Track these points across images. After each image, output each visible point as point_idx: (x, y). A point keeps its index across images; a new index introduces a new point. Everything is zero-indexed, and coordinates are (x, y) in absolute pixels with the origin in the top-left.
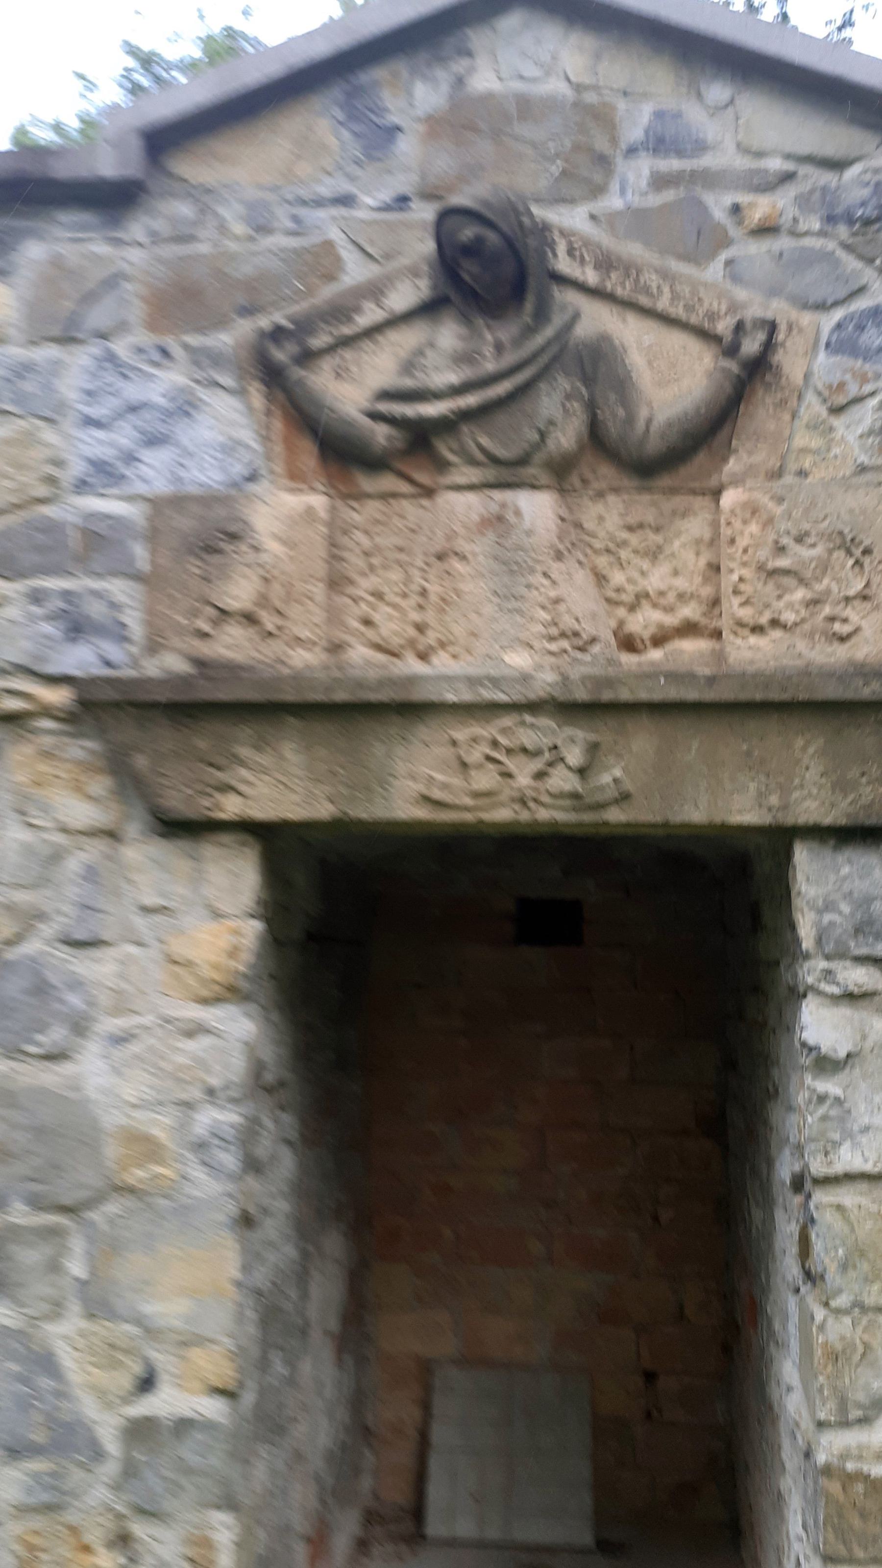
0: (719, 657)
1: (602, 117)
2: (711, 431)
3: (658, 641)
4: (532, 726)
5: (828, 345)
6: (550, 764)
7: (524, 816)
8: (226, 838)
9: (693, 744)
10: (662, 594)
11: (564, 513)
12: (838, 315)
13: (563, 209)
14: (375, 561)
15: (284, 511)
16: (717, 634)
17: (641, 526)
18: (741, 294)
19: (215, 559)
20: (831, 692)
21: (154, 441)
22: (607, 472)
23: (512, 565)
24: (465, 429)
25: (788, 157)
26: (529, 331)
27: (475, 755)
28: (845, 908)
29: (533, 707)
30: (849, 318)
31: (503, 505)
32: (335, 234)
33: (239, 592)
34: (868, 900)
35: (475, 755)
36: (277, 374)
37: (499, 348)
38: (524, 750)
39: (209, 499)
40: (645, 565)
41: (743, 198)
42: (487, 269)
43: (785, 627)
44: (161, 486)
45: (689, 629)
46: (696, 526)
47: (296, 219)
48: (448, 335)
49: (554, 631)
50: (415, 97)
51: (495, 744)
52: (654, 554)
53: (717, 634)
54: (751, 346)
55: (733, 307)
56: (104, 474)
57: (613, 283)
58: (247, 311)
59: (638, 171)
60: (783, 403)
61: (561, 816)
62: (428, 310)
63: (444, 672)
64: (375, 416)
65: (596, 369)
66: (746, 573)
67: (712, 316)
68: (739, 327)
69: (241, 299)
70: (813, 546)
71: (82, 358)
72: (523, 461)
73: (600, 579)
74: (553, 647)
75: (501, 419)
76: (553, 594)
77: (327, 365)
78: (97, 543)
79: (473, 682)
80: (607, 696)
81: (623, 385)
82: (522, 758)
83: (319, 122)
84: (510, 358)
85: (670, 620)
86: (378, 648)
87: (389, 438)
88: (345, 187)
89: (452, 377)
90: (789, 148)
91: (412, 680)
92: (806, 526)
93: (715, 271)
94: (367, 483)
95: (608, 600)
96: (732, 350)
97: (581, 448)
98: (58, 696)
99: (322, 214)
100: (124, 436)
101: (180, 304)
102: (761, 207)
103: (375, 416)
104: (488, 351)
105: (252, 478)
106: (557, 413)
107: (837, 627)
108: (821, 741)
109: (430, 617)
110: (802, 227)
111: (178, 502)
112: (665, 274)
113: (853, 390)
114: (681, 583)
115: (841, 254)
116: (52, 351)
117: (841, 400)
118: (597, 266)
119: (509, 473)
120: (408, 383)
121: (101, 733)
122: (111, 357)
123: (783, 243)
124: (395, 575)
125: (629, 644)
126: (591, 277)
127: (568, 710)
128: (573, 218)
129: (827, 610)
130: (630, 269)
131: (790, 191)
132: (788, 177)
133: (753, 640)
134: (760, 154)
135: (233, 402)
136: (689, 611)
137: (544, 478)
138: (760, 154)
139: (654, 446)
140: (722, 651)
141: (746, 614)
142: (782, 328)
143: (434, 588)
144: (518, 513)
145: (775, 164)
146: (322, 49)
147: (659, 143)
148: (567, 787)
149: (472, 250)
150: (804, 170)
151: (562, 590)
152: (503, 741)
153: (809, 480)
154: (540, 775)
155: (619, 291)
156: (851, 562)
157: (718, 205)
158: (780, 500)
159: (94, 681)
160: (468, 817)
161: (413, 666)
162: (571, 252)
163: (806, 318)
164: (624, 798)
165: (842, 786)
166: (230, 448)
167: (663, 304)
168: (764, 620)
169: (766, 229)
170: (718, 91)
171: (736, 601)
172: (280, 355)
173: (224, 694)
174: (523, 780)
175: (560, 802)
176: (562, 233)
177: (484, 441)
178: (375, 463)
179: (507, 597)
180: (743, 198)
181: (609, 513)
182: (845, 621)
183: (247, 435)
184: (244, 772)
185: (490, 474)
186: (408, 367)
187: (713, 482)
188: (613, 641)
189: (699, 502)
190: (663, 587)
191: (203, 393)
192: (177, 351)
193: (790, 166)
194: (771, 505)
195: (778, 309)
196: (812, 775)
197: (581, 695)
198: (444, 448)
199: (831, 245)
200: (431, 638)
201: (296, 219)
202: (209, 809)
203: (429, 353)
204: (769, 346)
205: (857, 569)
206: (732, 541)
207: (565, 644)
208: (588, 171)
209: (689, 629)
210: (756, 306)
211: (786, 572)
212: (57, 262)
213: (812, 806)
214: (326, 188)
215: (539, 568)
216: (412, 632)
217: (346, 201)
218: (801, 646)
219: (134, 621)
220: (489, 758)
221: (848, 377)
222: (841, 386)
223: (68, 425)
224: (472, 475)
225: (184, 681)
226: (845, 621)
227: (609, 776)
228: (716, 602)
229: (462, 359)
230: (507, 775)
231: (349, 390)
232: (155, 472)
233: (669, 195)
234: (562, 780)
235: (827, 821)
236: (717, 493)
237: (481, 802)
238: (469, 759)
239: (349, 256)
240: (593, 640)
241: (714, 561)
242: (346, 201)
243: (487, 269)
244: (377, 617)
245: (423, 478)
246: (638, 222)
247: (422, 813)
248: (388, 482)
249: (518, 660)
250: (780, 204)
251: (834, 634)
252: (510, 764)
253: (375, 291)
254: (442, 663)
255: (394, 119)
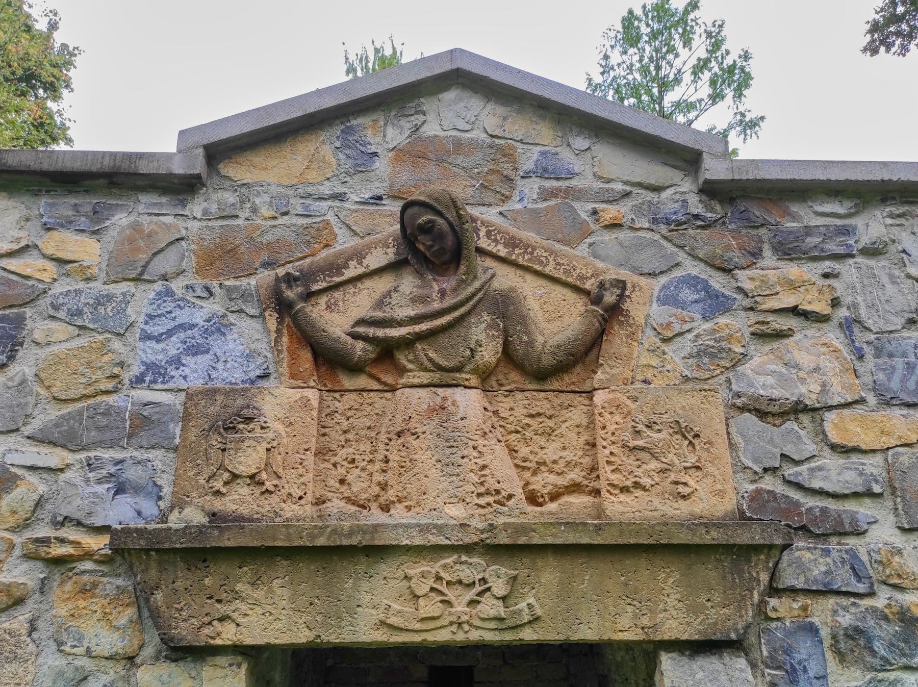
0: (600, 512)
1: (508, 154)
2: (584, 354)
3: (554, 497)
4: (466, 562)
5: (658, 300)
6: (480, 594)
7: (460, 637)
8: (222, 660)
9: (586, 576)
10: (555, 462)
11: (487, 405)
12: (663, 280)
13: (483, 209)
14: (350, 436)
15: (286, 402)
16: (597, 492)
17: (539, 414)
18: (600, 265)
19: (231, 436)
20: (684, 538)
21: (196, 350)
22: (514, 376)
23: (450, 440)
24: (418, 346)
25: (625, 183)
26: (462, 283)
27: (422, 588)
29: (467, 549)
30: (671, 282)
32: (330, 217)
33: (248, 460)
35: (422, 588)
36: (285, 307)
37: (443, 293)
38: (460, 582)
39: (231, 392)
40: (542, 441)
41: (600, 206)
42: (433, 242)
43: (644, 489)
44: (196, 383)
45: (574, 488)
46: (577, 416)
47: (306, 207)
48: (408, 284)
49: (482, 490)
50: (387, 136)
51: (439, 578)
52: (549, 434)
53: (597, 492)
54: (610, 298)
56: (154, 373)
57: (516, 255)
58: (267, 265)
60: (631, 336)
61: (490, 637)
62: (394, 267)
63: (399, 523)
65: (505, 309)
66: (613, 448)
67: (582, 278)
68: (601, 285)
70: (660, 431)
71: (149, 292)
72: (459, 369)
73: (512, 451)
74: (482, 501)
75: (443, 339)
76: (481, 462)
77: (323, 300)
78: (143, 423)
79: (423, 529)
81: (524, 320)
82: (460, 589)
83: (324, 147)
84: (449, 302)
85: (562, 481)
86: (348, 500)
87: (364, 350)
88: (341, 189)
90: (626, 178)
91: (376, 528)
93: (582, 250)
94: (348, 382)
95: (517, 466)
96: (597, 300)
97: (499, 360)
98: (98, 543)
99: (325, 204)
100: (173, 346)
101: (221, 258)
102: (610, 212)
103: (355, 336)
105: (264, 376)
106: (482, 337)
107: (681, 489)
108: (677, 575)
109: (390, 477)
110: (637, 226)
111: (210, 393)
112: (551, 252)
113: (677, 328)
114: (568, 455)
115: (662, 241)
117: (670, 334)
118: (506, 245)
119: (446, 377)
120: (380, 314)
121: (131, 571)
122: (169, 293)
123: (625, 235)
124: (366, 447)
125: (533, 499)
126: (503, 252)
127: (496, 551)
129: (672, 477)
130: (528, 247)
131: (629, 203)
132: (627, 194)
133: (623, 497)
134: (609, 181)
135: (256, 325)
136: (575, 475)
137: (474, 381)
138: (609, 181)
139: (547, 361)
140: (600, 504)
141: (615, 478)
142: (629, 285)
143: (394, 457)
144: (454, 403)
145: (618, 187)
146: (329, 102)
147: (543, 172)
148: (492, 613)
149: (428, 229)
150: (636, 191)
151: (487, 459)
152: (445, 575)
153: (652, 386)
154: (472, 603)
155: (520, 261)
156: (687, 442)
157: (583, 209)
158: (635, 400)
159: (127, 531)
160: (417, 638)
161: (377, 516)
162: (488, 234)
163: (643, 281)
164: (535, 620)
165: (695, 609)
166: (250, 356)
167: (549, 270)
168: (628, 483)
169: (615, 226)
170: (581, 143)
171: (609, 468)
172: (290, 294)
173: (229, 541)
174: (460, 608)
175: (487, 625)
176: (483, 223)
177: (432, 354)
178: (355, 369)
179: (447, 465)
180: (600, 206)
181: (517, 406)
182: (685, 484)
183: (262, 346)
184: (243, 607)
186: (380, 304)
187: (587, 387)
188: (523, 497)
189: (577, 399)
190: (555, 457)
191: (232, 318)
192: (216, 290)
194: (629, 402)
195: (624, 274)
196: (672, 601)
197: (503, 539)
198: (402, 358)
200: (391, 494)
201: (306, 207)
202: (212, 638)
204: (622, 297)
205: (690, 448)
206: (604, 428)
207: (490, 499)
209: (574, 488)
210: (612, 273)
211: (643, 449)
212: (136, 227)
213: (674, 627)
214: (325, 189)
215: (471, 443)
216: (377, 489)
217: (340, 197)
218: (656, 502)
219: (165, 481)
220: (432, 589)
222: (669, 324)
223: (133, 337)
224: (425, 378)
225: (201, 530)
226: (685, 484)
228: (593, 468)
230: (447, 603)
231: (336, 319)
232: (194, 374)
234: (490, 607)
235: (685, 637)
236: (590, 393)
237: (425, 626)
238: (419, 593)
239: (341, 233)
240: (510, 497)
241: (591, 439)
242: (340, 197)
243: (433, 242)
244: (350, 478)
245: (389, 379)
246: (534, 218)
247: (381, 636)
248: (363, 381)
249: (456, 512)
250: (623, 210)
251: (679, 493)
252: (451, 594)
253: (359, 255)
254: (399, 514)
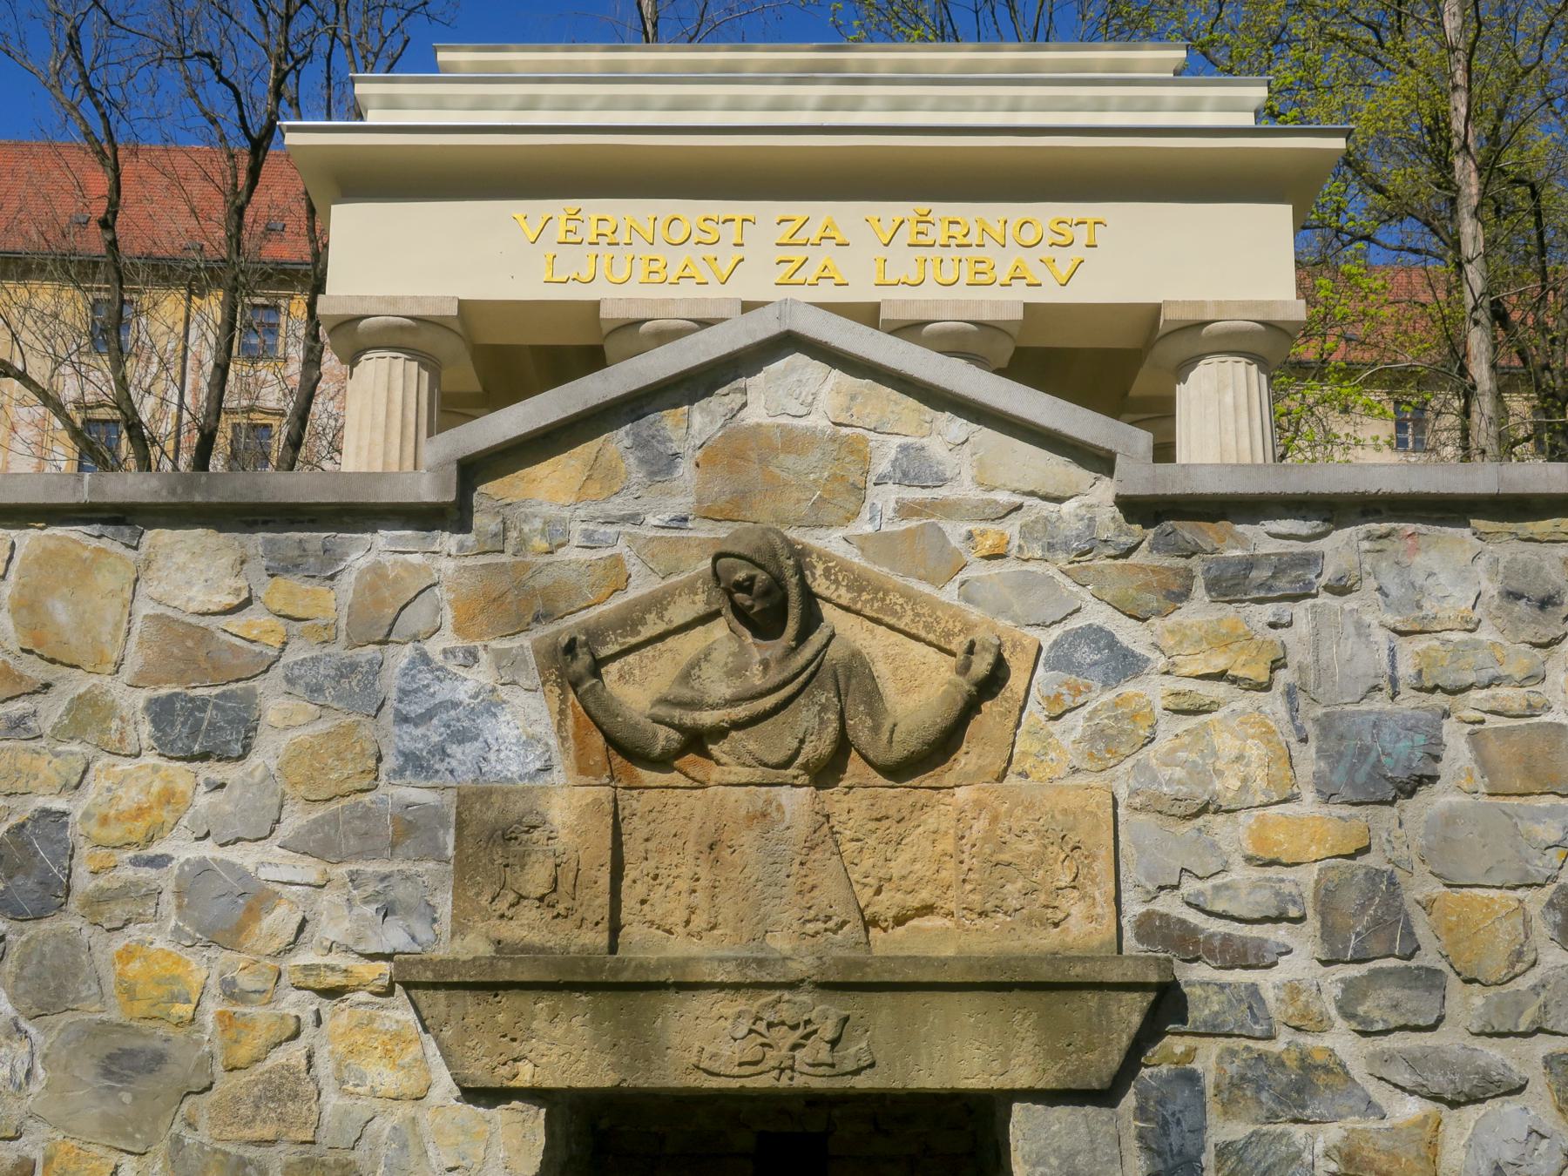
1: (857, 451)
7: (784, 1082)
12: (1056, 632)
18: (975, 614)
21: (461, 737)
28: (1054, 1161)
31: (768, 802)
33: (536, 878)
34: (1073, 1154)
36: (576, 666)
37: (765, 664)
55: (968, 627)
57: (864, 601)
59: (886, 498)
64: (658, 720)
65: (853, 681)
67: (948, 634)
69: (538, 606)
75: (766, 726)
80: (855, 977)
81: (873, 697)
84: (775, 677)
85: (914, 902)
89: (723, 690)
92: (1025, 823)
93: (949, 594)
100: (434, 733)
103: (658, 720)
104: (757, 669)
112: (910, 596)
113: (1068, 701)
115: (1060, 578)
116: (370, 651)
118: (849, 588)
120: (686, 694)
122: (425, 659)
123: (1009, 567)
125: (870, 923)
128: (830, 542)
129: (1042, 898)
139: (898, 752)
144: (779, 807)
145: (1004, 497)
157: (955, 531)
162: (827, 572)
165: (1054, 1054)
166: (530, 741)
168: (989, 906)
185: (758, 774)
193: (1017, 499)
196: (1027, 1046)
199: (1052, 571)
203: (704, 665)
208: (850, 493)
213: (1022, 1077)
217: (634, 519)
221: (1064, 690)
222: (1058, 696)
224: (744, 774)
227: (854, 1051)
229: (736, 671)
231: (636, 689)
233: (913, 523)
239: (634, 567)
242: (634, 519)
253: (657, 602)
255: (674, 447)
